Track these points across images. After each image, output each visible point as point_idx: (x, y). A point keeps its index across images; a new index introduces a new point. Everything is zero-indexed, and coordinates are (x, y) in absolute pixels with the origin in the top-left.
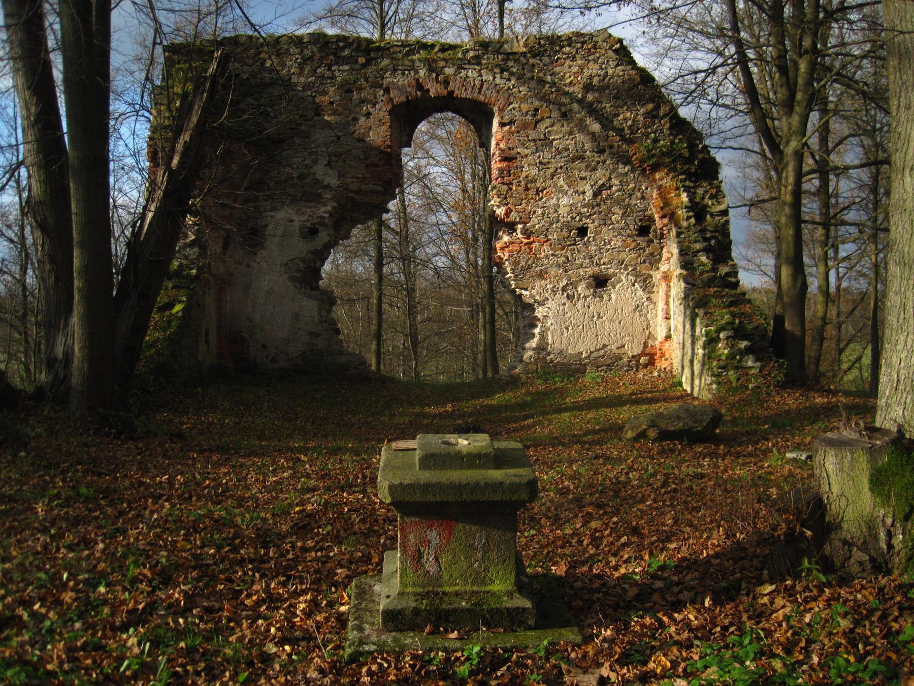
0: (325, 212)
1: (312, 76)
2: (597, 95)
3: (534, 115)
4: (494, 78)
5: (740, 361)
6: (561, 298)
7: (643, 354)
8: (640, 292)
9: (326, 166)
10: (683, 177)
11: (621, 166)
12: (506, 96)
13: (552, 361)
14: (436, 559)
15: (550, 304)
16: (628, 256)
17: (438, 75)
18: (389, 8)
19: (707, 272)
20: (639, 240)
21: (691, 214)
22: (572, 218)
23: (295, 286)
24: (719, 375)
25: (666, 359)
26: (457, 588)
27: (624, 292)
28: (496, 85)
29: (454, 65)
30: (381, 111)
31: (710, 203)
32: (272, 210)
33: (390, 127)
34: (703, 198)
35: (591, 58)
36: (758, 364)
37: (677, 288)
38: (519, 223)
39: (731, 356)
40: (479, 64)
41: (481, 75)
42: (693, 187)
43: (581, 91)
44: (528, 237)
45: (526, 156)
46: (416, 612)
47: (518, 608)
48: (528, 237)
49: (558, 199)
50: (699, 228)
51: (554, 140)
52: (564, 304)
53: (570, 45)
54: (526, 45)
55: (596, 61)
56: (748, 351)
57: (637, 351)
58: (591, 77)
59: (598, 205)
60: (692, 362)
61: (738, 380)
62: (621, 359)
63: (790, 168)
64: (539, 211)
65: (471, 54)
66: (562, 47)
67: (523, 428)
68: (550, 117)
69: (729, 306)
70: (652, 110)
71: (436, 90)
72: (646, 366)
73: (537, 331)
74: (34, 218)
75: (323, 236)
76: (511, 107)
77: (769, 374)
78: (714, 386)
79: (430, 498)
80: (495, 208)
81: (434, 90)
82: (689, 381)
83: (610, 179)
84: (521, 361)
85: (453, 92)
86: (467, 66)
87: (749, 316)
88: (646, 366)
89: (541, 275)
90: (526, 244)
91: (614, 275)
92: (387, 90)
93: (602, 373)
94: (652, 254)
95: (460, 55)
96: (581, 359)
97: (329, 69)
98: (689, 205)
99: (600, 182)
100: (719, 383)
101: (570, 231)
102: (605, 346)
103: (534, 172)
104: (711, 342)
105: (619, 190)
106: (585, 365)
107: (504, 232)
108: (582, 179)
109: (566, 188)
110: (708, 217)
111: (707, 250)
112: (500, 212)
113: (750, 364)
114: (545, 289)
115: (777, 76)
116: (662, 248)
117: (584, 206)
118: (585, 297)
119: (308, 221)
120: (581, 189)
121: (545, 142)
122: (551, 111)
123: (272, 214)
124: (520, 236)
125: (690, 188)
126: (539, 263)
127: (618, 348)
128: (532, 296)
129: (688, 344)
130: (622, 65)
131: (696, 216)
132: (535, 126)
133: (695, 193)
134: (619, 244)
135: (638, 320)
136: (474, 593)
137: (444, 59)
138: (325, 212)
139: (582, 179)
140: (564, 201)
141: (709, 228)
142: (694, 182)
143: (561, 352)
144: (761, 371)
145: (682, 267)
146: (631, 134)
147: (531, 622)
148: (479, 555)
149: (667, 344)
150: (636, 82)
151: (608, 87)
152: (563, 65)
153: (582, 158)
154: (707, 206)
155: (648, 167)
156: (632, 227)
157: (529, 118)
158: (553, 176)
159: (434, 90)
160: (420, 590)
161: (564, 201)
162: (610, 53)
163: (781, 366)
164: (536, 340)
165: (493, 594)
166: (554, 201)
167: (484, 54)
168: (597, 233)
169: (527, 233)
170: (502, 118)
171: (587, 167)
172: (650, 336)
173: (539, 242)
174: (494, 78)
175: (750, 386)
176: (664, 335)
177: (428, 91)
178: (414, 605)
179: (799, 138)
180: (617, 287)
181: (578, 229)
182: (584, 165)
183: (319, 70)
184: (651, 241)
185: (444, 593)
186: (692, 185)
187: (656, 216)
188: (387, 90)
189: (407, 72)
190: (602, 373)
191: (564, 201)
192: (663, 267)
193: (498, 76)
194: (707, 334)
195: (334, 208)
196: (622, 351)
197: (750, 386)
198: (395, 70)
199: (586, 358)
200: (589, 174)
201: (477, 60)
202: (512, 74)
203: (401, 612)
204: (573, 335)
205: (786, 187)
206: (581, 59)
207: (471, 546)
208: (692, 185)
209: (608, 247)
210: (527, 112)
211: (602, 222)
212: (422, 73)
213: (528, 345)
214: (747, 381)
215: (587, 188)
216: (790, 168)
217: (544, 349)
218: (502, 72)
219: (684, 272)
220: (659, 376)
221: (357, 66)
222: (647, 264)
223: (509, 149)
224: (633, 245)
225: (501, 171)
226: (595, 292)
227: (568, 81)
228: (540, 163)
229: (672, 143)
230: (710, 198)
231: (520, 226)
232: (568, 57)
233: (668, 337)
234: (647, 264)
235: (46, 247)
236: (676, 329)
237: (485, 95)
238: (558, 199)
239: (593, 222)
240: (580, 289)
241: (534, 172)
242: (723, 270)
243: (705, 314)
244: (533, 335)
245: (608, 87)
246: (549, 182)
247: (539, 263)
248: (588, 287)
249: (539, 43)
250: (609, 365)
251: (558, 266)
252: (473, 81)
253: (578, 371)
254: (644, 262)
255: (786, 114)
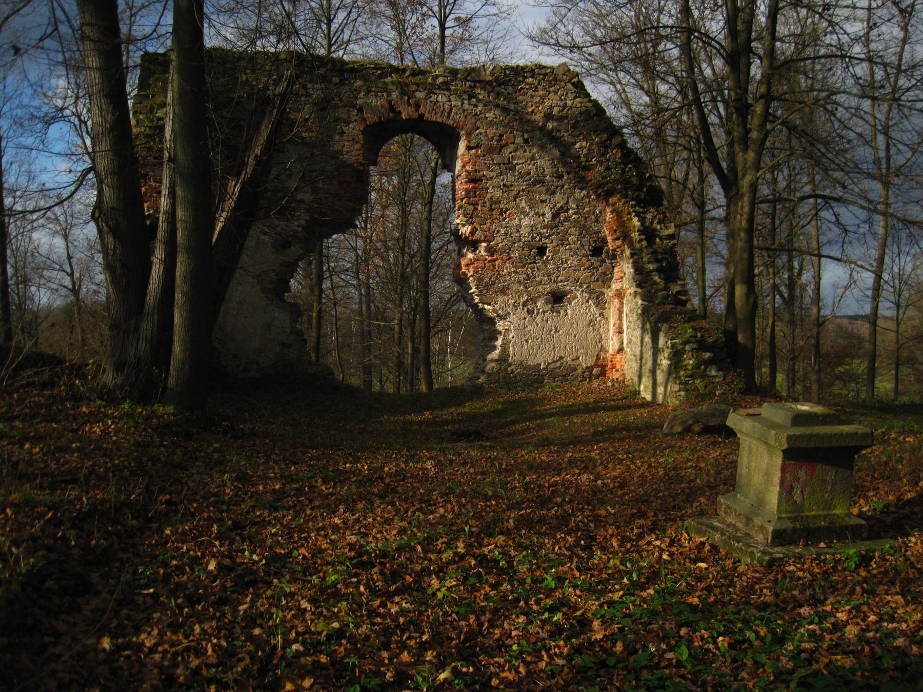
2: (556, 124)
3: (499, 140)
4: (463, 104)
5: (705, 370)
6: (521, 312)
7: (596, 365)
8: (594, 308)
10: (634, 203)
11: (577, 191)
12: (473, 120)
13: (512, 372)
14: (802, 492)
15: (511, 318)
16: (583, 275)
17: (409, 98)
19: (661, 290)
20: (593, 260)
21: (643, 237)
22: (533, 238)
23: (268, 298)
24: (686, 383)
25: (617, 371)
26: (813, 513)
27: (578, 308)
28: (464, 110)
30: (354, 129)
31: (658, 227)
33: (363, 145)
34: (652, 223)
35: (551, 89)
36: (721, 373)
37: (632, 305)
38: (484, 241)
39: (697, 367)
40: (448, 90)
41: (450, 101)
42: (643, 213)
43: (542, 120)
44: (492, 255)
45: (491, 178)
46: (795, 530)
47: (857, 525)
48: (492, 255)
49: (520, 220)
50: (651, 250)
51: (517, 164)
52: (525, 318)
53: (532, 77)
54: (492, 74)
55: (556, 93)
56: (708, 363)
57: (590, 363)
58: (551, 108)
59: (557, 226)
60: (653, 372)
61: (706, 387)
62: (576, 370)
63: (746, 199)
64: (503, 231)
65: (441, 80)
66: (525, 78)
67: (514, 433)
68: (514, 143)
69: (688, 322)
70: (606, 141)
71: (408, 112)
72: (598, 377)
73: (499, 342)
74: (106, 223)
75: (296, 249)
76: (478, 131)
77: (732, 382)
78: (682, 393)
79: (812, 445)
80: (460, 226)
81: (406, 112)
82: (650, 389)
83: (568, 202)
84: (483, 372)
85: (423, 115)
86: (438, 91)
87: (707, 330)
88: (598, 377)
89: (504, 291)
90: (490, 261)
91: (570, 292)
92: (360, 110)
93: (559, 383)
94: (604, 273)
95: (430, 80)
96: (539, 370)
98: (642, 228)
99: (559, 205)
100: (687, 391)
101: (531, 250)
102: (561, 358)
103: (498, 193)
104: (676, 356)
105: (575, 213)
106: (543, 375)
107: (468, 250)
108: (542, 201)
109: (527, 209)
110: (657, 240)
111: (659, 270)
112: (465, 230)
113: (713, 373)
114: (506, 304)
115: (735, 116)
116: (613, 268)
117: (544, 227)
118: (544, 312)
120: (541, 211)
121: (509, 166)
122: (515, 137)
124: (483, 253)
125: (640, 213)
126: (502, 279)
127: (573, 360)
128: (495, 311)
129: (648, 355)
130: (579, 97)
131: (647, 239)
132: (500, 151)
133: (645, 218)
134: (575, 263)
135: (591, 334)
136: (825, 516)
137: (415, 84)
139: (542, 201)
140: (526, 222)
141: (659, 250)
142: (643, 208)
143: (521, 364)
144: (724, 379)
145: (638, 286)
146: (587, 161)
147: (865, 535)
148: (829, 488)
149: (618, 357)
150: (592, 114)
151: (567, 117)
152: (525, 94)
153: (542, 182)
154: (656, 230)
155: (604, 193)
156: (586, 248)
157: (494, 143)
158: (515, 198)
159: (406, 112)
160: (790, 515)
161: (525, 223)
162: (569, 86)
163: (739, 375)
164: (497, 352)
165: (838, 516)
166: (516, 222)
167: (452, 81)
168: (556, 252)
169: (490, 251)
170: (469, 142)
171: (547, 191)
172: (603, 349)
173: (502, 259)
174: (463, 104)
175: (717, 393)
176: (616, 348)
177: (400, 113)
178: (791, 525)
179: (754, 172)
180: (573, 303)
181: (538, 248)
182: (544, 189)
184: (604, 261)
185: (807, 517)
186: (641, 210)
187: (609, 239)
188: (360, 110)
189: (380, 94)
190: (559, 383)
191: (526, 222)
192: (615, 286)
193: (466, 102)
194: (673, 346)
195: (307, 221)
196: (577, 362)
197: (717, 393)
198: (368, 91)
199: (544, 369)
200: (548, 197)
201: (446, 86)
202: (479, 101)
203: (784, 531)
204: (532, 348)
205: (742, 215)
206: (543, 90)
207: (825, 481)
208: (641, 210)
209: (565, 265)
210: (493, 137)
211: (560, 242)
212: (394, 95)
213: (490, 357)
214: (714, 388)
215: (547, 210)
216: (746, 199)
217: (506, 360)
218: (469, 99)
219: (639, 290)
220: (613, 385)
222: (600, 282)
223: (476, 171)
224: (587, 264)
225: (468, 191)
226: (553, 307)
227: (530, 110)
228: (504, 185)
229: (623, 171)
230: (658, 223)
231: (484, 244)
232: (531, 88)
233: (621, 350)
234: (600, 282)
235: (118, 252)
236: (630, 341)
237: (454, 119)
238: (520, 220)
239: (552, 242)
240: (539, 304)
241: (498, 193)
242: (675, 288)
243: (670, 328)
244: (495, 348)
245: (567, 117)
246: (512, 204)
247: (502, 279)
248: (546, 303)
249: (505, 73)
250: (565, 376)
251: (519, 282)
252: (444, 106)
253: (537, 381)
254: (598, 280)
255: (742, 150)
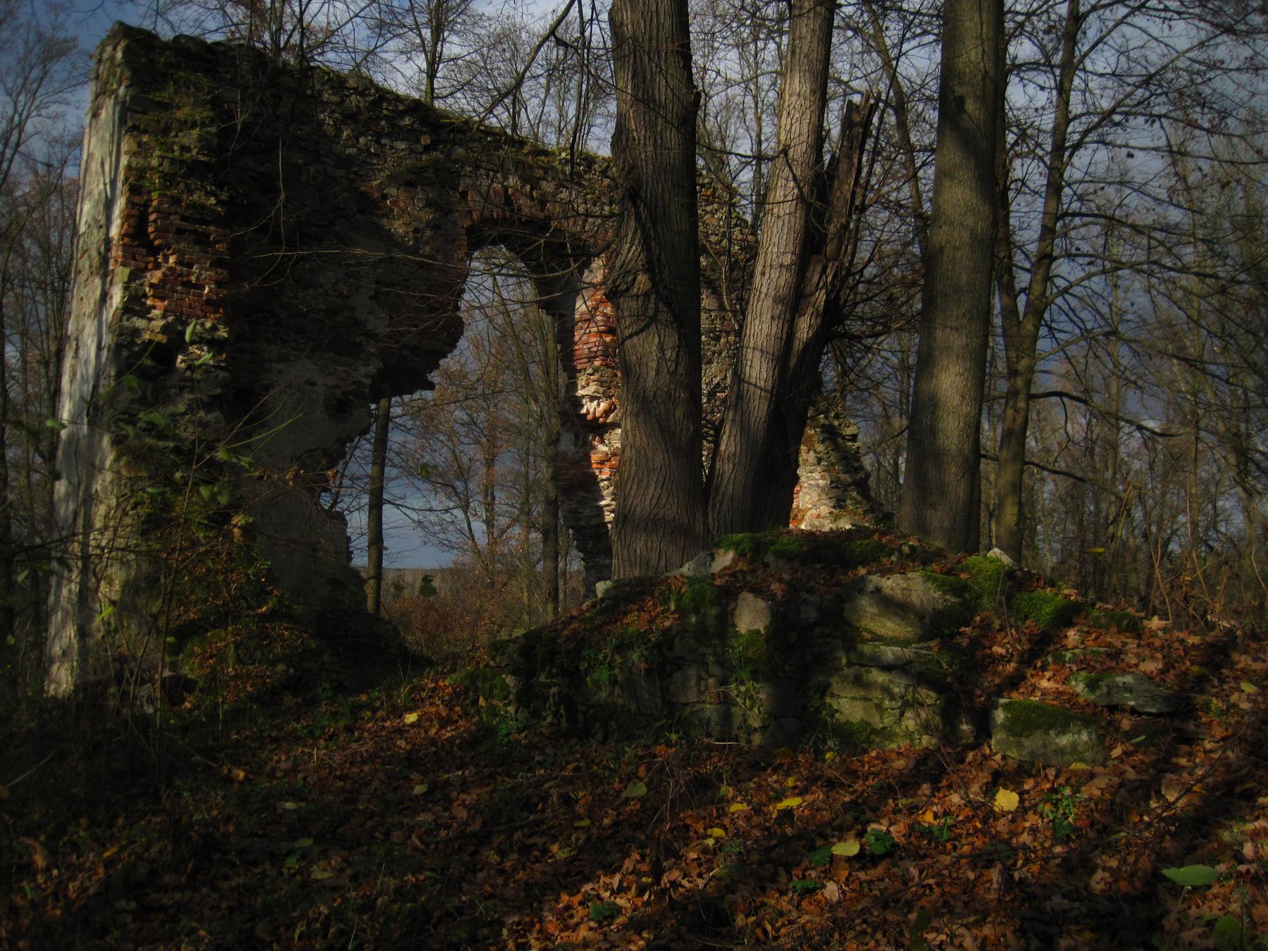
0: (366, 376)
1: (353, 146)
9: (371, 298)
17: (532, 189)
18: (61, 237)
29: (554, 179)
32: (279, 361)
97: (378, 142)
99: (716, 381)
119: (337, 386)
123: (281, 366)
138: (366, 376)
183: (362, 140)
189: (491, 174)
221: (419, 148)
